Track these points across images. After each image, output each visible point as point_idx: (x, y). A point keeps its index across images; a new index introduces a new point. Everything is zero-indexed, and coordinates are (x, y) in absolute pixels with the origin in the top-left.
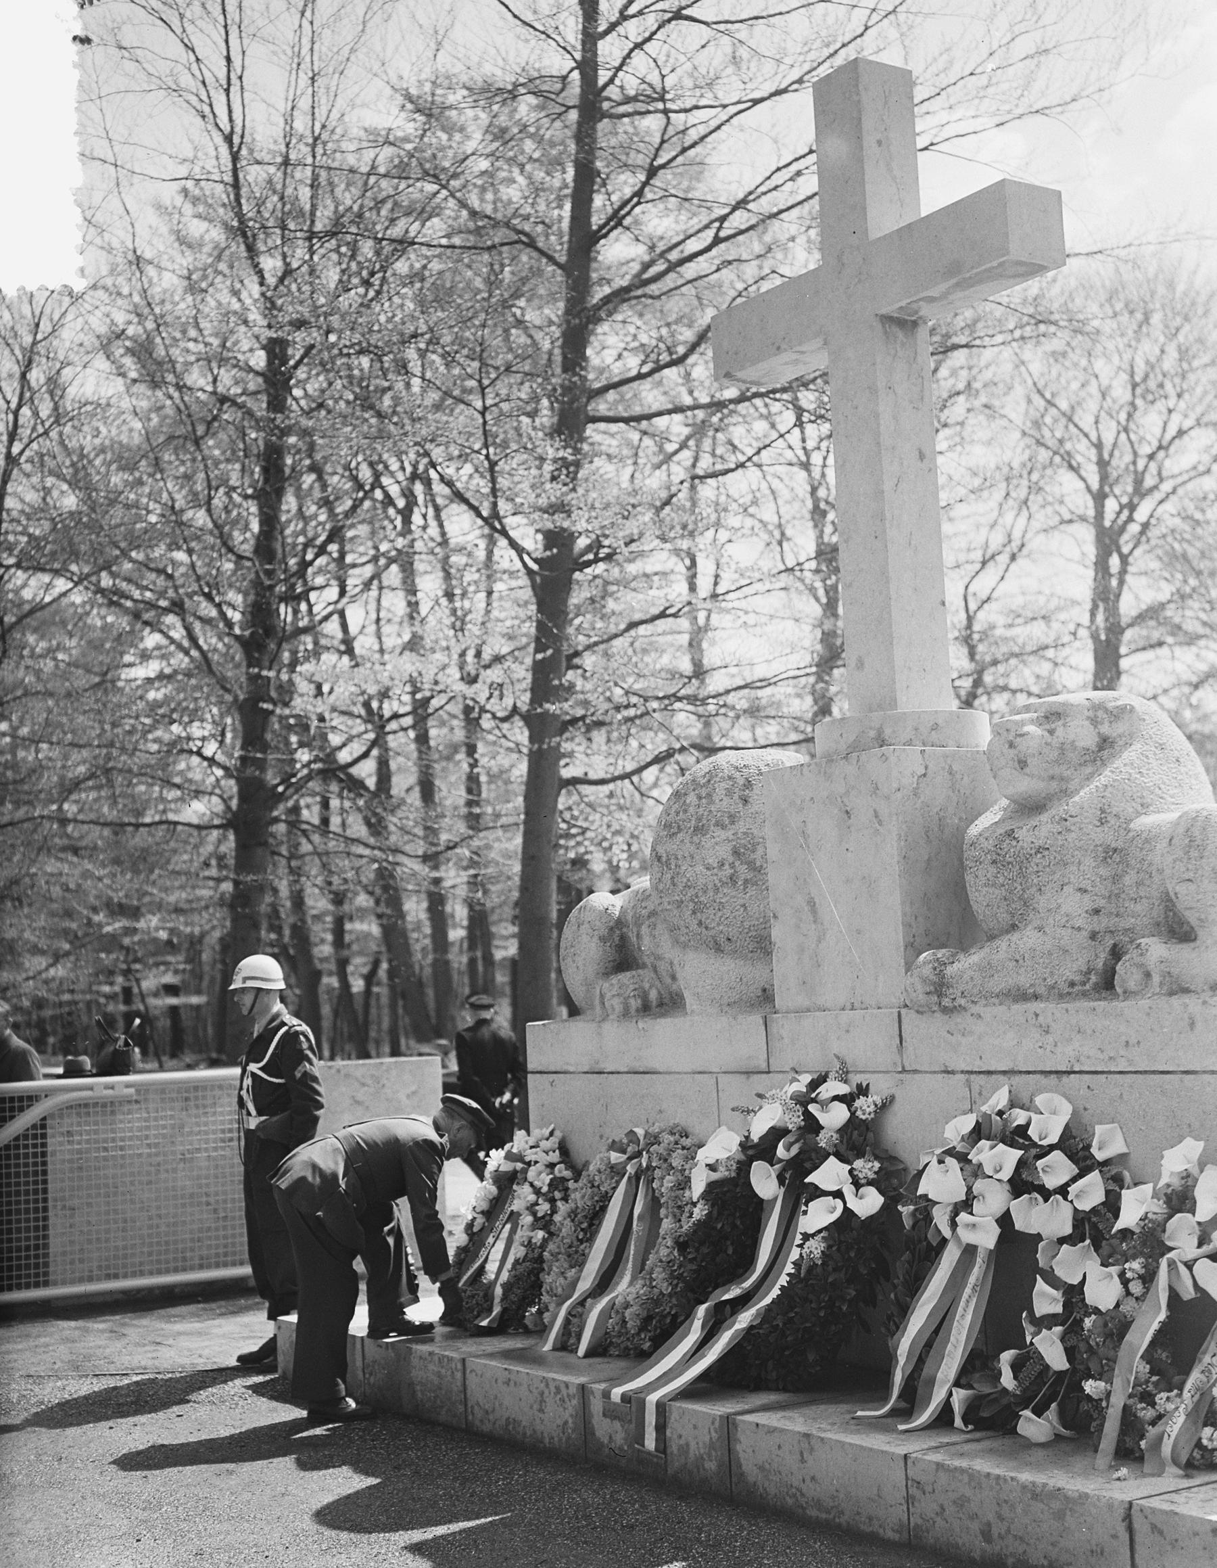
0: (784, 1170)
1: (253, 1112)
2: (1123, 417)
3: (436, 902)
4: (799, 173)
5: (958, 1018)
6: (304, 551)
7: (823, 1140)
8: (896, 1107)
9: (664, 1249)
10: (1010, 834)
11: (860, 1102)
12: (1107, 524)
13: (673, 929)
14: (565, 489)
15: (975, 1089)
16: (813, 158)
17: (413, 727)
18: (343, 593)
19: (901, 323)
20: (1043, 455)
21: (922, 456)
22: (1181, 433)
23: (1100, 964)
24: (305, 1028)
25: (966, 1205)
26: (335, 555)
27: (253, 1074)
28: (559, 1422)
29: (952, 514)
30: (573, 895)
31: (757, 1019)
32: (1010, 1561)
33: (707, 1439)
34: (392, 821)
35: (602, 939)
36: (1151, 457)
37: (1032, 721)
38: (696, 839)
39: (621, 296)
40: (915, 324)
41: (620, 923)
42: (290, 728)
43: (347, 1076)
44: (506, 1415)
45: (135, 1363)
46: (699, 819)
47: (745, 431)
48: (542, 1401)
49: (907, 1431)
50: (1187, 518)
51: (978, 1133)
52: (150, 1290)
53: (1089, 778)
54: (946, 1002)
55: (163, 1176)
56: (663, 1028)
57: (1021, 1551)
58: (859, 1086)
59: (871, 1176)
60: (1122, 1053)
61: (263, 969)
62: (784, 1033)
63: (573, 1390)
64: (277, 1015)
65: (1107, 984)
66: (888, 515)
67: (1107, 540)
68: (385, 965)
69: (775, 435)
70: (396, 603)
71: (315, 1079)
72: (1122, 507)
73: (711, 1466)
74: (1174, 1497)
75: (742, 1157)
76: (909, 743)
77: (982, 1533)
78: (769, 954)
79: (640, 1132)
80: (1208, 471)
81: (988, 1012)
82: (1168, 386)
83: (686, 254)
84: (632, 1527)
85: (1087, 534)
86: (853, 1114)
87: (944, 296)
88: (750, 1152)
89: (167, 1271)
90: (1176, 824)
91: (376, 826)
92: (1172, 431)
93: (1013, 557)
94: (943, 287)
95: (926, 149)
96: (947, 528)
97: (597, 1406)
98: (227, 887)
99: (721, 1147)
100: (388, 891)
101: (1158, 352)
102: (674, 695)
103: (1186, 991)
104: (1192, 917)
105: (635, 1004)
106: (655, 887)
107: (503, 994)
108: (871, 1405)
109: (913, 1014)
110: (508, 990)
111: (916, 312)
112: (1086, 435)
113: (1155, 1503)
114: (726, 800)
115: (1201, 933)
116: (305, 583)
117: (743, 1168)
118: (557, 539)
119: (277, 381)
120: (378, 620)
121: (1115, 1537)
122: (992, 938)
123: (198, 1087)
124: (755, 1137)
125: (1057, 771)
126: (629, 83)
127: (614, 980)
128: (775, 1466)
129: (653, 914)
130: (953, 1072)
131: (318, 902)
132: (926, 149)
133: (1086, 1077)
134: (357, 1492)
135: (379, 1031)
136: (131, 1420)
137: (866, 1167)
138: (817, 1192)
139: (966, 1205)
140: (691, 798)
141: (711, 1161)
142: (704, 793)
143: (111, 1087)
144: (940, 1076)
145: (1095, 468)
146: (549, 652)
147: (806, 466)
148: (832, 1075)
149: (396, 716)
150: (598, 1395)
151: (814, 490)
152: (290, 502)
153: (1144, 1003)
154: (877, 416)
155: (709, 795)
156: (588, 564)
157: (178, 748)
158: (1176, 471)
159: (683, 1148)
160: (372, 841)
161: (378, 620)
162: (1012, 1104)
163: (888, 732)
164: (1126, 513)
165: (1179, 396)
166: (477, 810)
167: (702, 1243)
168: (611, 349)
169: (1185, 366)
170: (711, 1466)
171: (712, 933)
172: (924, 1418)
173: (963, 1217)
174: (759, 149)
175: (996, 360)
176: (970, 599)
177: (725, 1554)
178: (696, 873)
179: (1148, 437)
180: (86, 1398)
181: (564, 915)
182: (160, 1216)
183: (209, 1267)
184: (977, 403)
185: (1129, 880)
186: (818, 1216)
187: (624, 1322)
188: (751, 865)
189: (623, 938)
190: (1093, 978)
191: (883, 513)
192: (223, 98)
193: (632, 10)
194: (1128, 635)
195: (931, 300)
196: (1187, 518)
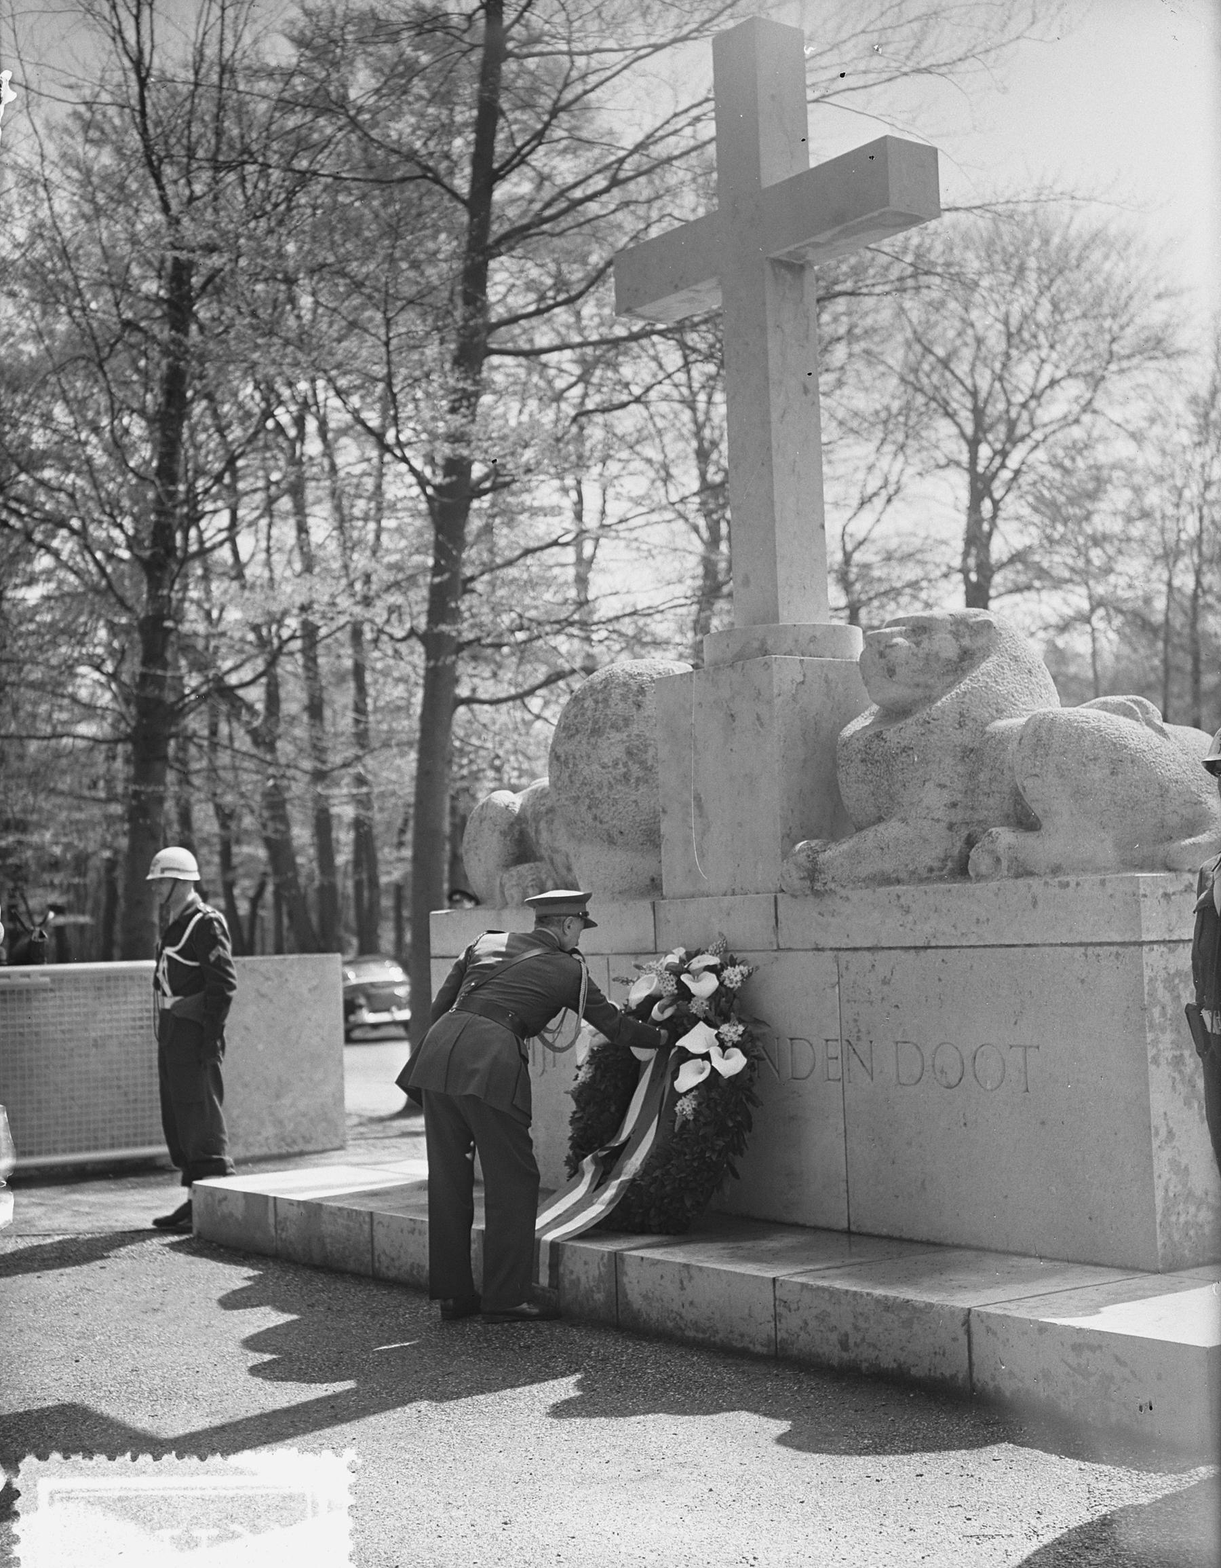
2: (998, 366)
3: (323, 824)
4: (697, 119)
10: (879, 736)
13: (570, 823)
14: (464, 421)
15: (843, 964)
16: (712, 105)
19: (789, 266)
20: (920, 400)
21: (806, 391)
22: (1053, 383)
23: (956, 852)
27: (169, 958)
29: (833, 457)
31: (646, 904)
32: (865, 1365)
33: (597, 1273)
35: (504, 834)
36: (1024, 405)
37: (900, 634)
38: (593, 740)
41: (520, 819)
43: (253, 970)
44: (410, 1261)
45: (56, 1226)
46: (596, 722)
47: (635, 370)
50: (1060, 466)
52: (63, 1167)
53: (950, 686)
54: (818, 886)
55: (77, 1060)
59: (736, 1039)
64: (192, 903)
65: (962, 870)
66: (774, 444)
67: (980, 487)
68: (270, 888)
69: (661, 376)
70: (286, 532)
72: (995, 453)
73: (599, 1297)
74: (1008, 1305)
77: (840, 1342)
78: (658, 846)
82: (1042, 338)
83: (589, 192)
84: (529, 1347)
85: (957, 485)
86: (721, 983)
89: (80, 1150)
91: (264, 740)
92: (1044, 381)
93: (889, 500)
94: (828, 234)
100: (276, 803)
101: (1031, 303)
103: (1031, 874)
104: (1037, 809)
106: (553, 784)
107: (387, 919)
110: (392, 914)
112: (962, 383)
114: (621, 705)
115: (1045, 823)
119: (178, 309)
120: (268, 550)
121: (955, 1339)
122: (860, 829)
123: (110, 977)
125: (921, 679)
127: (513, 871)
128: (657, 1293)
129: (551, 810)
130: (822, 950)
133: (941, 951)
134: (276, 1327)
136: (57, 1272)
140: (589, 703)
142: (600, 698)
143: (27, 975)
145: (969, 415)
146: (446, 576)
147: (691, 405)
153: (993, 884)
154: (765, 352)
155: (605, 700)
158: (1046, 419)
161: (268, 550)
163: (770, 642)
165: (1052, 347)
168: (506, 283)
169: (1058, 318)
170: (599, 1297)
171: (606, 826)
175: (878, 311)
176: (847, 538)
178: (591, 771)
179: (1022, 386)
180: (13, 1254)
182: (72, 1098)
183: (120, 1146)
184: (857, 348)
185: (982, 777)
186: (689, 1077)
188: (642, 763)
189: (522, 832)
190: (950, 864)
192: (132, 22)
194: (998, 579)
195: (817, 245)
196: (1060, 466)
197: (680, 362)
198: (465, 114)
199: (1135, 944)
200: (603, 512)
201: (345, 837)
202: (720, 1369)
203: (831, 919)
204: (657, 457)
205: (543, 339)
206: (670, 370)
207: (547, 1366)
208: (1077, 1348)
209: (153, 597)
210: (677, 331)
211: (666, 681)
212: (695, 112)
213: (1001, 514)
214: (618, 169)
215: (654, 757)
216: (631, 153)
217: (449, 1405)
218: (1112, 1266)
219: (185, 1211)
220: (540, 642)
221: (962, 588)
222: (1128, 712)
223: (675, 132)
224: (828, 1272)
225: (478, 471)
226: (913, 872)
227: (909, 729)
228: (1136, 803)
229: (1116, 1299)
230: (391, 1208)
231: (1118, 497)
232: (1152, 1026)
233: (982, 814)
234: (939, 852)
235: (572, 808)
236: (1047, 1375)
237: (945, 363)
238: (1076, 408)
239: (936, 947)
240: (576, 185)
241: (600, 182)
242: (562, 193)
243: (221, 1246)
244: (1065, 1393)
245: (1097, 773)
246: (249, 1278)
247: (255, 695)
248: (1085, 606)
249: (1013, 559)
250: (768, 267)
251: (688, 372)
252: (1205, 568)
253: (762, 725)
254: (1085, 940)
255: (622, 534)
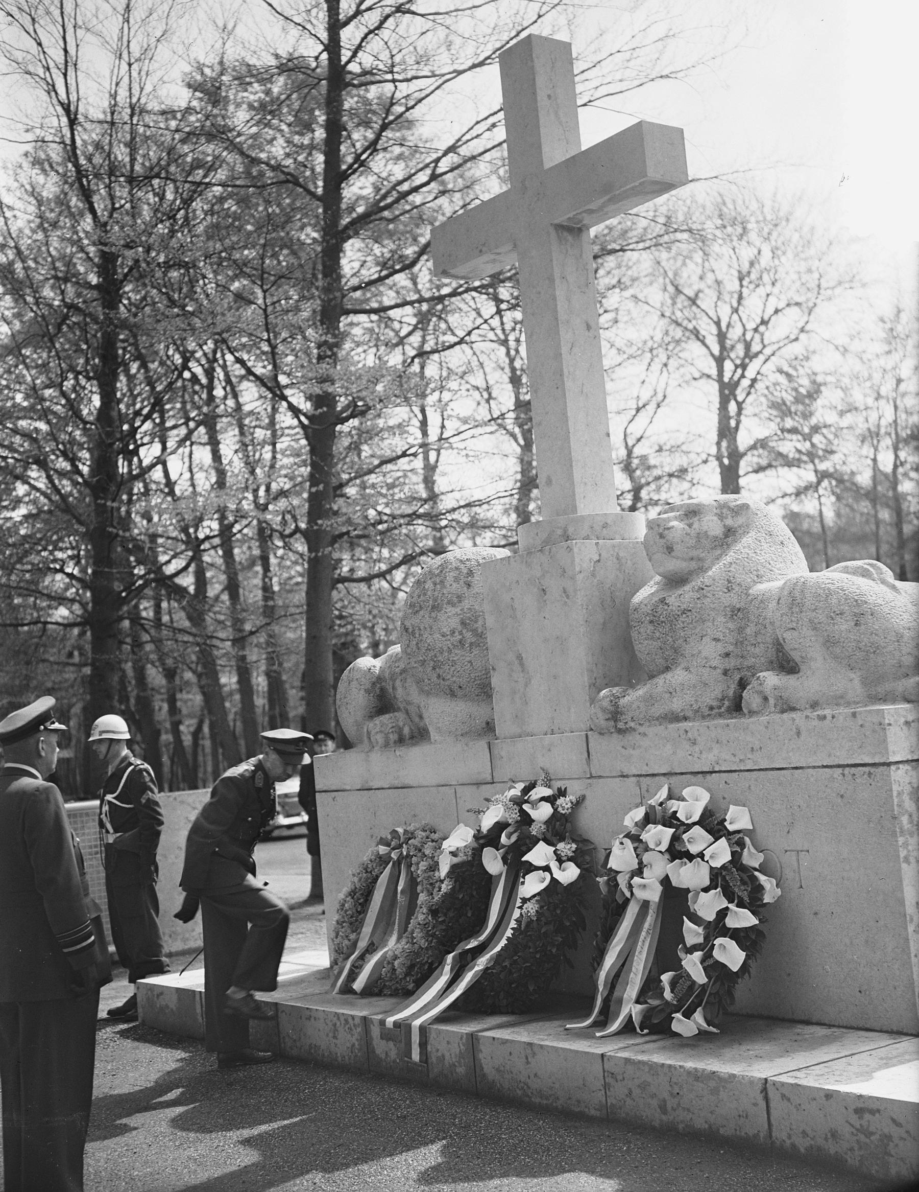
0: (507, 853)
1: (111, 831)
4: (494, 125)
5: (630, 738)
6: (134, 419)
7: (534, 830)
8: (587, 802)
9: (420, 916)
11: (560, 801)
12: (726, 380)
13: (419, 682)
16: (501, 115)
17: (222, 545)
18: (164, 448)
21: (589, 327)
22: (777, 311)
23: (731, 693)
24: (146, 766)
25: (639, 872)
26: (158, 421)
27: (109, 802)
28: (349, 1045)
29: (614, 376)
30: (346, 653)
31: (482, 744)
32: (681, 1126)
34: (209, 618)
35: (367, 691)
36: (756, 330)
37: (676, 518)
39: (364, 219)
40: (580, 230)
41: (379, 679)
42: (130, 552)
43: (182, 802)
47: (460, 319)
48: (336, 1030)
49: (602, 1037)
51: (648, 819)
53: (718, 558)
54: (621, 725)
56: (415, 753)
57: (688, 1117)
58: (559, 789)
59: (570, 854)
60: (750, 756)
61: (114, 725)
62: (503, 753)
63: (357, 1021)
64: (126, 758)
65: (737, 707)
66: (565, 371)
67: (727, 391)
69: (479, 321)
70: (203, 455)
71: (157, 804)
72: (737, 367)
73: (461, 1070)
75: (476, 845)
76: (587, 538)
77: (660, 1107)
78: (490, 697)
79: (400, 830)
80: (797, 339)
81: (652, 731)
86: (555, 810)
87: (601, 208)
88: (482, 841)
90: (782, 588)
91: (196, 618)
92: (770, 310)
93: (659, 406)
95: (585, 105)
96: (609, 386)
97: (375, 1031)
98: (87, 670)
99: (460, 838)
102: (414, 513)
103: (793, 709)
104: (796, 656)
105: (393, 737)
106: (404, 651)
108: (576, 1017)
109: (596, 736)
111: (581, 221)
113: (784, 1079)
114: (455, 585)
116: (136, 441)
117: (477, 853)
118: (323, 400)
119: (109, 292)
121: (755, 1105)
122: (652, 677)
124: (485, 830)
125: (695, 553)
126: (366, 59)
127: (378, 720)
128: (508, 1067)
129: (404, 671)
130: (627, 776)
131: (155, 676)
132: (585, 105)
135: (205, 772)
137: (566, 848)
138: (531, 868)
139: (639, 872)
140: (429, 585)
141: (453, 849)
144: (618, 779)
147: (505, 342)
148: (539, 782)
149: (208, 538)
150: (376, 1024)
151: (512, 361)
152: (122, 383)
153: (764, 719)
154: (554, 299)
155: (442, 582)
156: (347, 419)
157: (45, 570)
159: (433, 841)
160: (194, 630)
162: (670, 797)
163: (571, 530)
164: (739, 371)
165: (773, 284)
166: (271, 603)
167: (448, 910)
168: (356, 259)
169: (776, 261)
170: (461, 1070)
172: (615, 1026)
173: (636, 880)
174: (459, 112)
175: (640, 261)
177: (474, 1132)
178: (433, 639)
179: (753, 316)
181: (337, 679)
184: (627, 293)
185: (748, 631)
186: (532, 885)
187: (394, 970)
188: (475, 631)
189: (382, 689)
190: (727, 703)
191: (562, 370)
193: (363, 7)
194: (743, 463)
195: (591, 212)
197: (494, 309)
198: (320, 134)
199: (884, 764)
200: (443, 427)
201: (260, 681)
202: (562, 1132)
203: (632, 752)
204: (481, 384)
205: (389, 298)
206: (486, 317)
207: (419, 1134)
208: (859, 1111)
209: (101, 510)
210: (490, 288)
211: (490, 564)
212: (491, 120)
213: (744, 412)
214: (436, 166)
215: (484, 625)
216: (445, 154)
217: (339, 1175)
218: (881, 1031)
219: (132, 1003)
220: (396, 532)
221: (718, 470)
222: (865, 574)
223: (477, 136)
224: (647, 1046)
225: (342, 402)
226: (697, 711)
227: (686, 595)
228: (877, 648)
229: (887, 1063)
230: (292, 999)
231: (830, 396)
232: (902, 832)
233: (751, 661)
234: (718, 693)
235: (420, 669)
236: (834, 1134)
237: (693, 301)
238: (796, 332)
239: (720, 772)
240: (405, 180)
241: (422, 178)
242: (394, 188)
243: (160, 1031)
244: (852, 1149)
245: (844, 626)
246: (181, 1060)
247: (187, 581)
248: (813, 478)
249: (753, 447)
250: (552, 231)
251: (501, 317)
252: (901, 446)
253: (568, 597)
254: (841, 763)
255: (454, 446)
